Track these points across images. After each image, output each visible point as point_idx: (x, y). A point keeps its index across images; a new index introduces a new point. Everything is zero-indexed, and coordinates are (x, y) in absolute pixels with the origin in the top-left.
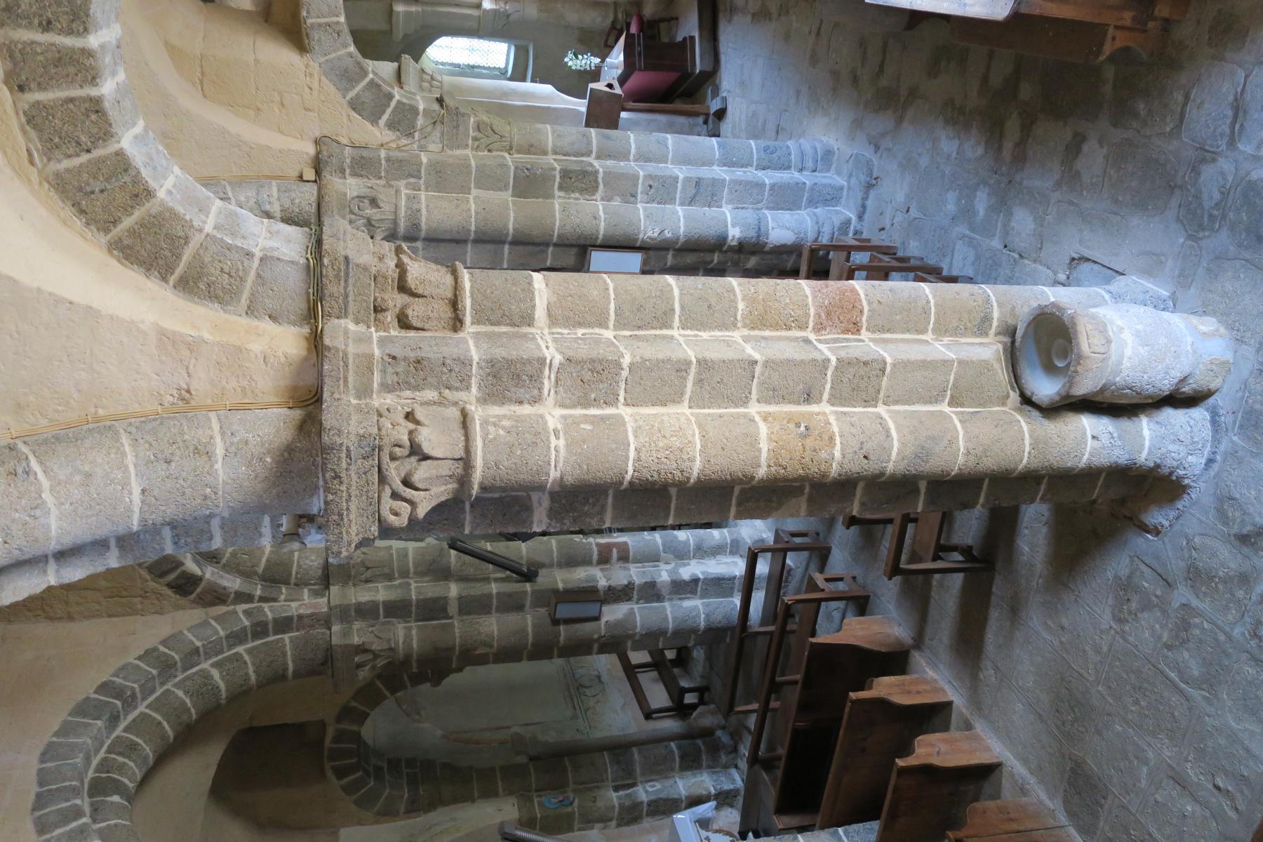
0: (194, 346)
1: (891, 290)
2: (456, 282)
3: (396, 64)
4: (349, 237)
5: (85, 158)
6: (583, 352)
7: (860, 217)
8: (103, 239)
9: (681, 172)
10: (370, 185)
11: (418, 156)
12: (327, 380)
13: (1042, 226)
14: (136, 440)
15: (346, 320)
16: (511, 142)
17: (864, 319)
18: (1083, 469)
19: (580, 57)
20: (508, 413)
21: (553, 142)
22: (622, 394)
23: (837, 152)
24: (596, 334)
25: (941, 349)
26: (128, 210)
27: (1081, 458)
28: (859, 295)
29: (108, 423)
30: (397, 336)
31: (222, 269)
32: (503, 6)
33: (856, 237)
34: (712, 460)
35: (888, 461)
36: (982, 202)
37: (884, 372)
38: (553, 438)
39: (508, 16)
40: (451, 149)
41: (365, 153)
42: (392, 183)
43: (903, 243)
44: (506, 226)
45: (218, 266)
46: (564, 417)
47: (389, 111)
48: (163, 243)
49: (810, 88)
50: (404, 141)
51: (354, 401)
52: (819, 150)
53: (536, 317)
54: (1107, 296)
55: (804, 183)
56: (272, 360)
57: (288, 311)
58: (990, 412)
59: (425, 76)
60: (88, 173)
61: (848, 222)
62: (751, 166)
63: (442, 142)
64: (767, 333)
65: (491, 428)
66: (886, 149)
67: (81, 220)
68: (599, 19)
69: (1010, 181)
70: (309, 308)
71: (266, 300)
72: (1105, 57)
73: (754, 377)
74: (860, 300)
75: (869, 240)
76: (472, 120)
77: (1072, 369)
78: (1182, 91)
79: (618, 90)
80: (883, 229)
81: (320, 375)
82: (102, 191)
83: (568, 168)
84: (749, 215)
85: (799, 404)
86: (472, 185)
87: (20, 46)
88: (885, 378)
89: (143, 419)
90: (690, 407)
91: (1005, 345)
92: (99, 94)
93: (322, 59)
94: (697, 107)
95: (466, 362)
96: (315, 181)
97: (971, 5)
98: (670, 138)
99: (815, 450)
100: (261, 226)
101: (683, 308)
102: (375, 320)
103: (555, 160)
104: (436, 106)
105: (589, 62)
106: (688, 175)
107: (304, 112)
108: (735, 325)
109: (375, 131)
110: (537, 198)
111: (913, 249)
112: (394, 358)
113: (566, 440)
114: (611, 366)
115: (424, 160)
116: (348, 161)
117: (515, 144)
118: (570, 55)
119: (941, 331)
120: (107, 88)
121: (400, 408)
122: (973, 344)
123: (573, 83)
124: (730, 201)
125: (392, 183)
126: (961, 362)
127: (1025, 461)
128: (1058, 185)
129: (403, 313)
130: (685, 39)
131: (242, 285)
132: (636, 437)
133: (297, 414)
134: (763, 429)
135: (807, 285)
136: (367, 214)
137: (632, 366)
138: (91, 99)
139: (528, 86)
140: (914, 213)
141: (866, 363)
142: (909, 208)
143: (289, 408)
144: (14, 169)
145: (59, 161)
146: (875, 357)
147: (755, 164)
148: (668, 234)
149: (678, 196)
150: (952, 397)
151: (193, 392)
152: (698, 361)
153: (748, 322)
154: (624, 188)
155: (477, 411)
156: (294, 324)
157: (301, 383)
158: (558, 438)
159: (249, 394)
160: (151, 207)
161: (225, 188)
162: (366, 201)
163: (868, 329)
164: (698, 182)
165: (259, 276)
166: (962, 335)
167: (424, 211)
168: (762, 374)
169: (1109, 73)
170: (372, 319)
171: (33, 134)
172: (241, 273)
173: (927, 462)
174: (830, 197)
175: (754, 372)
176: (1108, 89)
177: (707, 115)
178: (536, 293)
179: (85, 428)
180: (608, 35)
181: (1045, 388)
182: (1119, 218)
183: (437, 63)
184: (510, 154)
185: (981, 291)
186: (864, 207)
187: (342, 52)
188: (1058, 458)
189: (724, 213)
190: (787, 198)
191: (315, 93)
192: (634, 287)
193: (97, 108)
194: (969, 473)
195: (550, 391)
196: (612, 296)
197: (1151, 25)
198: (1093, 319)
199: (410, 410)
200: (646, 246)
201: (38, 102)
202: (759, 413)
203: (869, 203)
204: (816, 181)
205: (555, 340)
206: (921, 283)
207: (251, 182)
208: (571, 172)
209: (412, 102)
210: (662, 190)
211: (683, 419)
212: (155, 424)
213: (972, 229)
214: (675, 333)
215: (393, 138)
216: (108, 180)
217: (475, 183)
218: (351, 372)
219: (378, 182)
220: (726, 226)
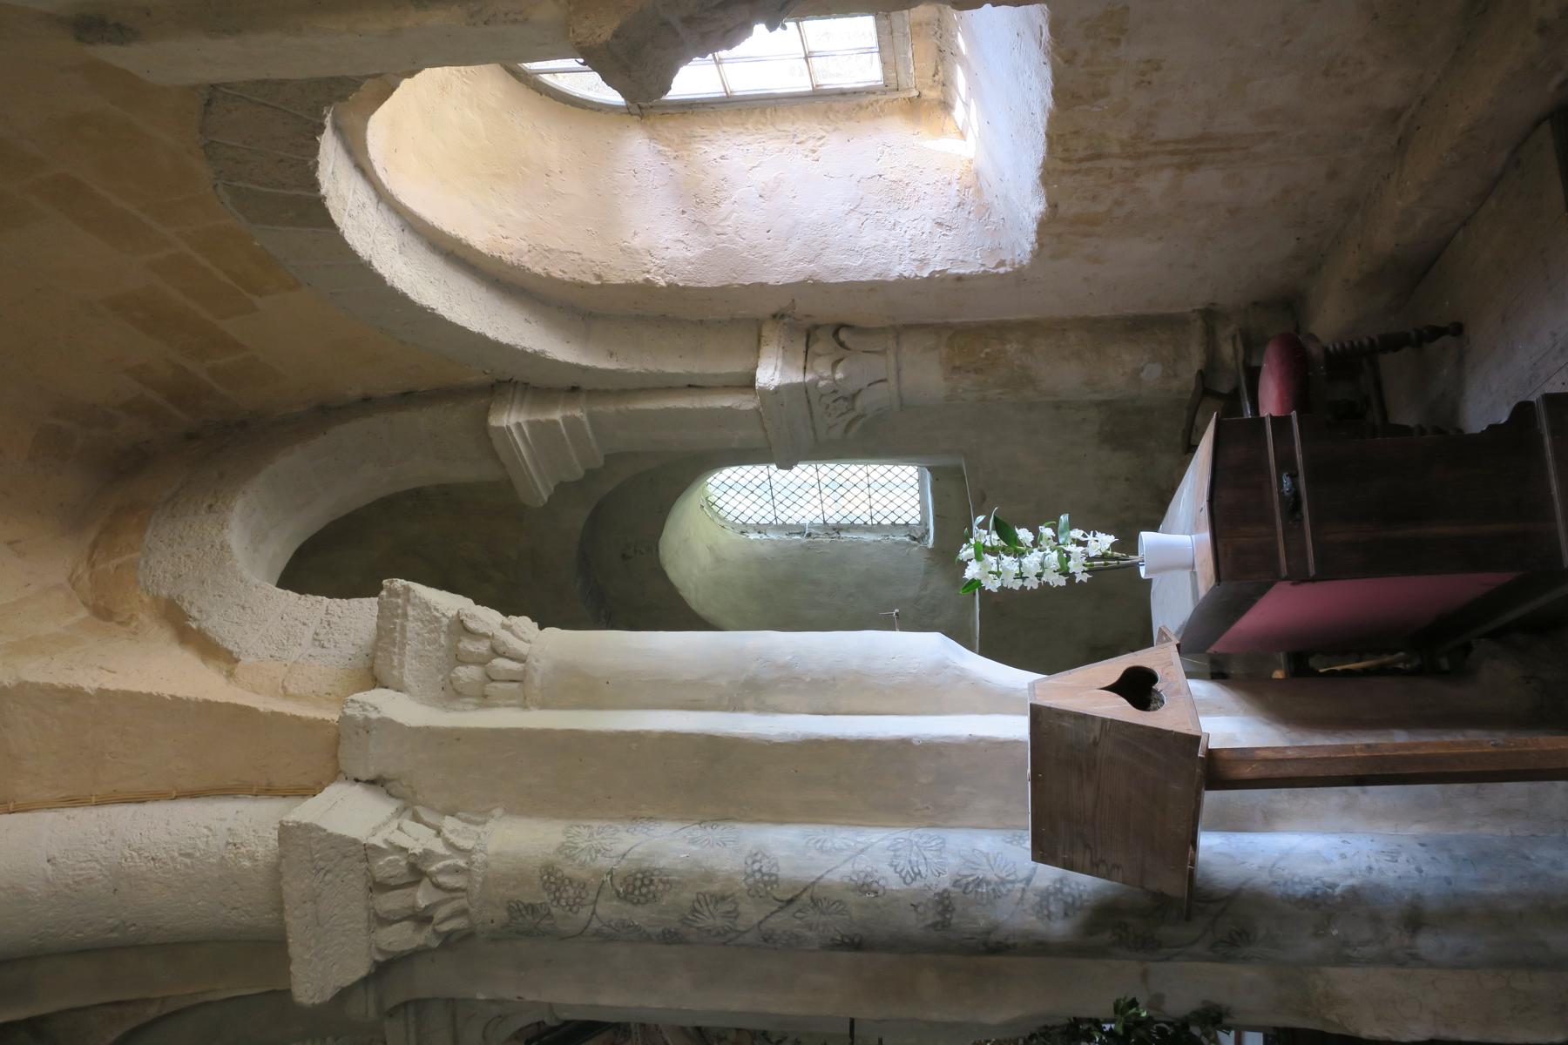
19: (1024, 535)
32: (827, 373)
59: (468, 645)
68: (1153, 372)
130: (1523, 412)
180: (1193, 410)
183: (744, 529)
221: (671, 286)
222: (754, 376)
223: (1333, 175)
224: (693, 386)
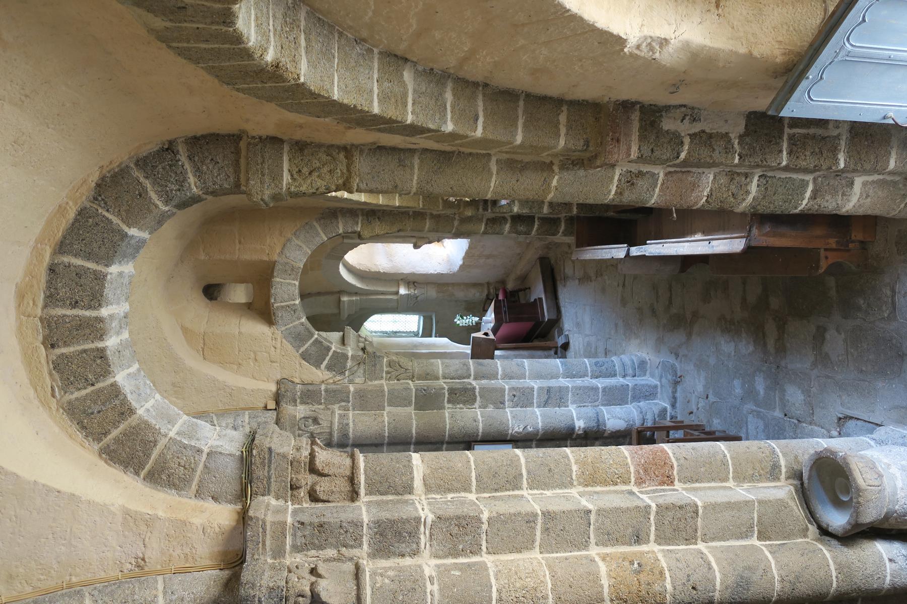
0: (150, 522)
1: (693, 449)
2: (353, 463)
3: (341, 333)
4: (275, 436)
5: (90, 389)
6: (452, 511)
7: (673, 406)
8: (96, 447)
9: (536, 384)
10: (313, 409)
11: (348, 387)
12: (249, 544)
13: (809, 396)
14: (97, 601)
15: (269, 497)
16: (413, 373)
17: (675, 472)
18: (889, 590)
19: (465, 318)
20: (393, 565)
21: (442, 370)
22: (484, 544)
23: (649, 362)
24: (462, 497)
25: (742, 492)
26: (115, 425)
27: (884, 580)
28: (668, 454)
29: (79, 588)
30: (308, 508)
31: (179, 463)
32: (413, 291)
33: (673, 420)
34: (562, 596)
35: (714, 591)
36: (760, 385)
37: (697, 514)
38: (428, 583)
39: (417, 297)
40: (371, 380)
41: (311, 388)
42: (329, 406)
43: (708, 421)
44: (410, 431)
45: (176, 460)
46: (438, 566)
47: (328, 358)
48: (138, 447)
49: (623, 321)
50: (338, 378)
51: (270, 561)
52: (635, 361)
53: (415, 486)
54: (872, 443)
55: (628, 385)
56: (209, 531)
57: (226, 493)
58: (795, 543)
59: (360, 339)
60: (90, 400)
61: (664, 410)
62: (587, 376)
63: (365, 377)
64: (598, 489)
65: (379, 579)
66: (683, 356)
67: (82, 433)
68: (478, 295)
69: (778, 367)
70: (242, 489)
71: (211, 485)
72: (823, 270)
73: (590, 524)
74: (669, 458)
75: (682, 422)
76: (385, 360)
77: (855, 500)
78: (889, 288)
79: (492, 336)
80: (692, 413)
81: (245, 541)
82: (99, 412)
83: (454, 387)
84: (589, 411)
85: (631, 545)
86: (386, 404)
87: (55, 319)
88: (699, 519)
89: (106, 584)
90: (541, 553)
91: (795, 486)
92: (104, 346)
93: (283, 328)
94: (548, 343)
95: (359, 523)
96: (276, 409)
97: (717, 246)
98: (526, 362)
99: (649, 584)
100: (213, 432)
101: (529, 472)
102: (292, 496)
103: (444, 383)
104: (361, 353)
105: (471, 320)
106: (541, 386)
107: (270, 363)
108: (572, 484)
109: (319, 372)
110: (433, 410)
111: (717, 424)
112: (303, 524)
113: (439, 585)
114: (473, 521)
115: (352, 388)
116: (299, 394)
117: (416, 374)
118: (458, 317)
119: (740, 478)
120: (111, 342)
121: (307, 565)
122: (769, 487)
123: (461, 335)
124: (574, 402)
125: (329, 406)
126: (760, 502)
127: (834, 585)
128: (814, 364)
129: (313, 488)
130: (535, 300)
131: (193, 474)
132: (497, 580)
133: (226, 573)
134: (603, 568)
135: (626, 449)
136: (311, 429)
137: (490, 520)
138: (98, 349)
139: (433, 340)
140: (712, 398)
141: (681, 507)
142: (708, 395)
143: (220, 569)
144: (41, 401)
145: (72, 393)
146: (688, 502)
147: (590, 374)
148: (530, 429)
149: (535, 401)
150: (759, 532)
151: (147, 560)
152: (543, 513)
153: (582, 480)
154: (495, 399)
155: (368, 564)
156: (230, 503)
157: (231, 549)
158: (432, 584)
159: (190, 559)
160: (132, 421)
161: (212, 419)
162: (310, 420)
163: (680, 481)
164: (549, 390)
165: (205, 466)
166: (759, 481)
167: (351, 425)
168: (597, 521)
169: (831, 282)
170: (289, 495)
171: (57, 376)
172: (193, 466)
173: (748, 590)
174: (648, 394)
175: (589, 520)
176: (833, 293)
177: (557, 348)
178: (415, 468)
179: (59, 593)
181: (838, 520)
182: (867, 383)
183: (372, 332)
184: (412, 381)
185: (767, 445)
186: (675, 398)
187: (297, 322)
188: (864, 581)
189: (570, 410)
190: (616, 396)
191: (278, 351)
192: (490, 459)
193: (101, 355)
194: (788, 598)
195: (426, 544)
196: (473, 467)
197: (851, 246)
198: (862, 458)
199: (314, 566)
200: (515, 439)
201: (62, 354)
202: (598, 554)
203: (678, 395)
204: (636, 383)
205: (429, 504)
206: (717, 443)
207: (231, 413)
208: (455, 389)
209: (345, 352)
210: (523, 398)
211: (535, 563)
212: (113, 587)
213: (758, 405)
214: (524, 492)
215: (331, 376)
216: (103, 404)
217: (388, 403)
218: (268, 537)
219: (319, 407)
220: (573, 420)
221: (384, 272)
222: (398, 292)
223: (510, 261)
224: (383, 293)
